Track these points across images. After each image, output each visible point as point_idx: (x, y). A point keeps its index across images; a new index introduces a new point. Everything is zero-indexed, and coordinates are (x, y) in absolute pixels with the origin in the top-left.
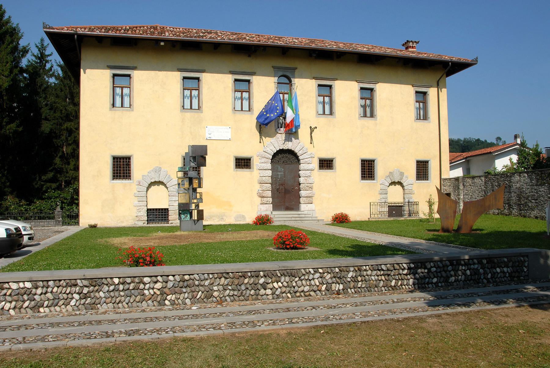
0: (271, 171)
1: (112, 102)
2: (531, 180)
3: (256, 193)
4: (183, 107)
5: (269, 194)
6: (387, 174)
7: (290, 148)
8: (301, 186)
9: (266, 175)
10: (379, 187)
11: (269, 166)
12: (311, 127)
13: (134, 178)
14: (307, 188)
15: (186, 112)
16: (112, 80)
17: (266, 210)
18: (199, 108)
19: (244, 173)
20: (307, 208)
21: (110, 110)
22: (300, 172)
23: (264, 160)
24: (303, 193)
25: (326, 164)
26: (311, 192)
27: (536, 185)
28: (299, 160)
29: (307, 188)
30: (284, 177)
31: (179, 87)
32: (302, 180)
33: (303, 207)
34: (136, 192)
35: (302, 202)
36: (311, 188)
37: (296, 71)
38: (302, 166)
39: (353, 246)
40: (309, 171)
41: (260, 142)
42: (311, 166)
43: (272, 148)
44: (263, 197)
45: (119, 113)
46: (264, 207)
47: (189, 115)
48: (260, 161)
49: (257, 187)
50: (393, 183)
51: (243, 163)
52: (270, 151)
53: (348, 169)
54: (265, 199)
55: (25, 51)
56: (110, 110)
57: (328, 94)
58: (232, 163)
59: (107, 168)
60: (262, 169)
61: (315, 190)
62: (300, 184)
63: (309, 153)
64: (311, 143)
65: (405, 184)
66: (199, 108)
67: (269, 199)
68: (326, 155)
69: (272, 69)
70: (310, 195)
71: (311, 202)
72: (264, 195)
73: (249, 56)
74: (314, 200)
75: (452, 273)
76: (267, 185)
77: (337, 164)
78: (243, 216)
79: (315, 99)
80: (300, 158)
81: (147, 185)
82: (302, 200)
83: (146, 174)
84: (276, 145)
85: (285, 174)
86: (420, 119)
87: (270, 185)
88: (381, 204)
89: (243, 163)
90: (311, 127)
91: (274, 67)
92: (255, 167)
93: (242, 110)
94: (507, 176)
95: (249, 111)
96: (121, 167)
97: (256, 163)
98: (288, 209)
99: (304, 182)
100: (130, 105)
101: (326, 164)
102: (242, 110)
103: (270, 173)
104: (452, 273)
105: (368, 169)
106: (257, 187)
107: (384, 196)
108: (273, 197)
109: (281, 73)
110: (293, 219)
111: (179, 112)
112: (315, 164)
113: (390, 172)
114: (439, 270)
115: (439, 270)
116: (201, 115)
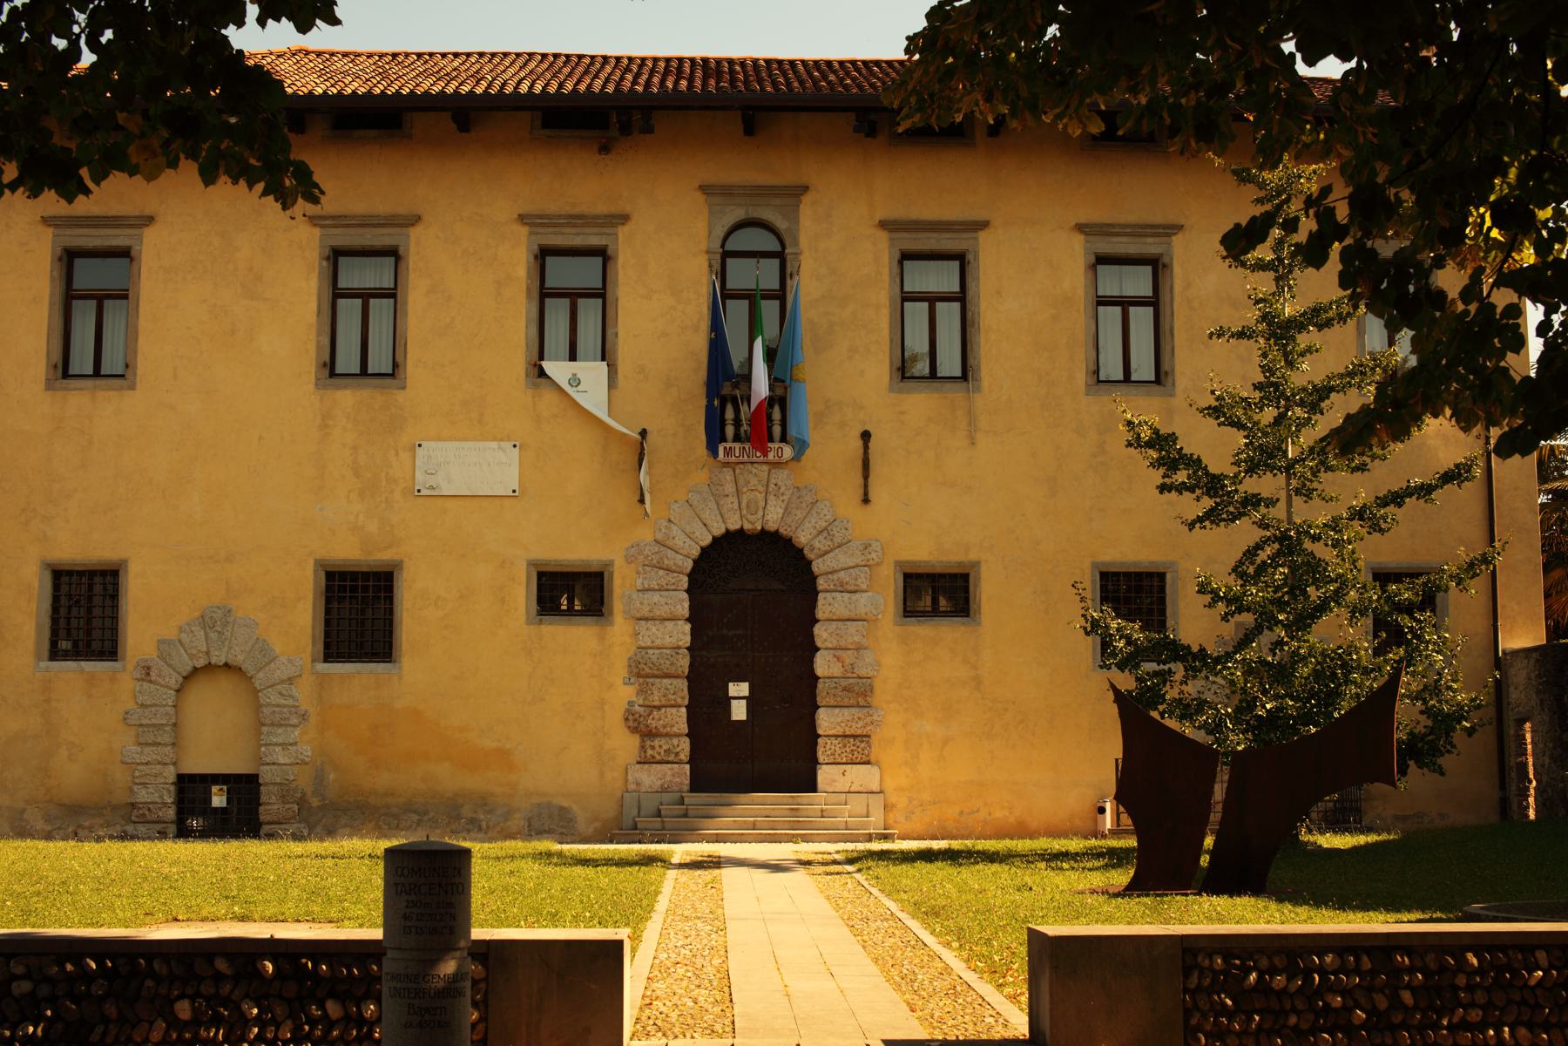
1: (57, 356)
4: (1097, 372)
13: (129, 653)
15: (338, 387)
16: (896, 269)
19: (574, 636)
21: (49, 386)
23: (661, 577)
24: (827, 720)
25: (940, 593)
31: (315, 291)
34: (130, 705)
37: (807, 199)
40: (857, 627)
42: (862, 603)
45: (79, 399)
46: (650, 778)
47: (347, 398)
51: (568, 592)
57: (1145, 290)
58: (522, 595)
60: (653, 619)
66: (966, 374)
68: (926, 552)
73: (605, 149)
75: (111, 1010)
81: (174, 680)
83: (171, 633)
89: (568, 592)
91: (705, 189)
93: (1127, 378)
99: (836, 670)
100: (395, 365)
101: (940, 593)
102: (1127, 378)
104: (111, 1010)
106: (624, 694)
109: (737, 214)
111: (311, 387)
112: (885, 597)
114: (44, 990)
115: (44, 990)
116: (401, 397)
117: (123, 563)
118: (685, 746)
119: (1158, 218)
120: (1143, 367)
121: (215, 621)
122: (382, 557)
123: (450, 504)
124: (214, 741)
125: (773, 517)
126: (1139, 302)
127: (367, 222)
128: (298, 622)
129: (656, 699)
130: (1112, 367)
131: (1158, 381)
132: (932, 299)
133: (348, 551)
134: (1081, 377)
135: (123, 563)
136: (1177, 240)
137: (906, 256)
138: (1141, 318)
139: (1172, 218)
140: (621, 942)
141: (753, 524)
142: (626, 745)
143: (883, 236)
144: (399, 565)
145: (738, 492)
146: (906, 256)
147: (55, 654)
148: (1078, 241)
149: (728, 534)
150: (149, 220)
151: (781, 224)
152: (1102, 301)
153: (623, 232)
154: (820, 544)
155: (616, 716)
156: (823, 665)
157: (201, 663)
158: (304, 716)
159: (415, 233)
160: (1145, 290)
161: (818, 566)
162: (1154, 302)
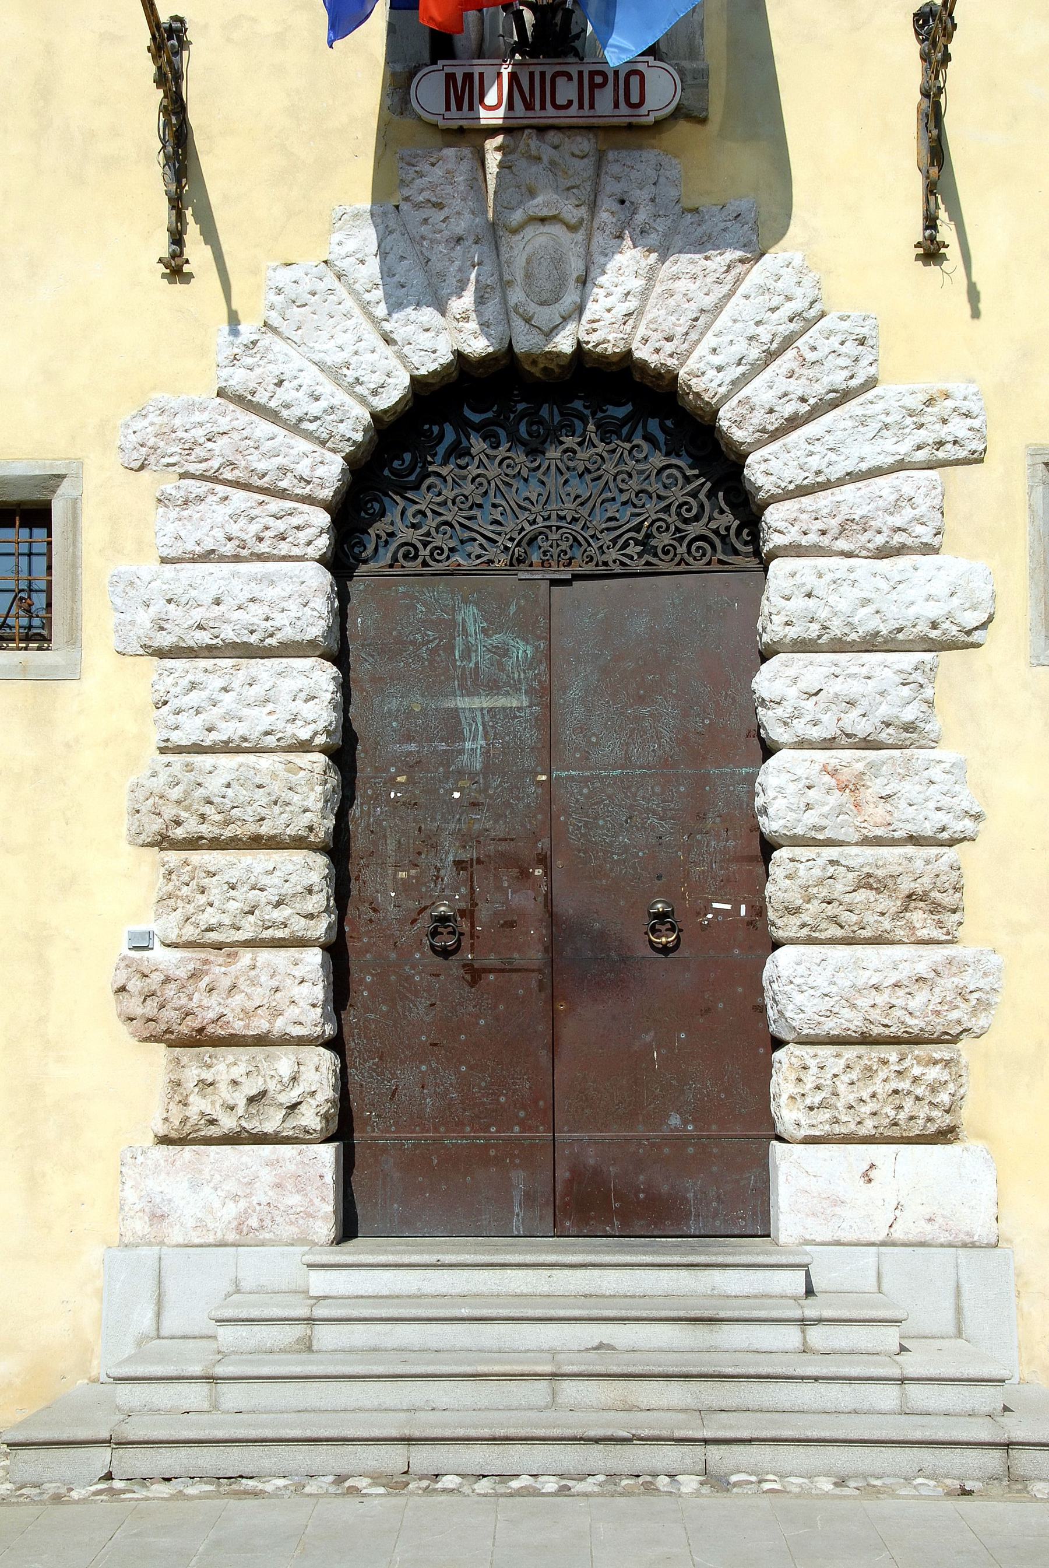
3: (108, 978)
5: (296, 988)
8: (786, 878)
9: (254, 723)
11: (299, 595)
14: (874, 910)
17: (244, 1237)
20: (867, 1212)
22: (767, 681)
23: (221, 516)
24: (801, 982)
26: (925, 959)
28: (749, 509)
29: (874, 910)
30: (548, 750)
32: (785, 792)
33: (815, 1188)
35: (788, 1114)
36: (936, 905)
38: (788, 593)
41: (176, 270)
44: (199, 1039)
48: (170, 530)
52: (307, 390)
54: (228, 1065)
55: (498, 149)
56: (1034, 452)
62: (768, 847)
63: (894, 394)
64: (931, 253)
67: (284, 1061)
70: (917, 1011)
71: (922, 1115)
72: (209, 1008)
74: (988, 1081)
76: (259, 861)
80: (763, 470)
82: (793, 1085)
85: (547, 719)
98: (599, 1205)
99: (825, 810)
106: (122, 896)
110: (588, 1403)
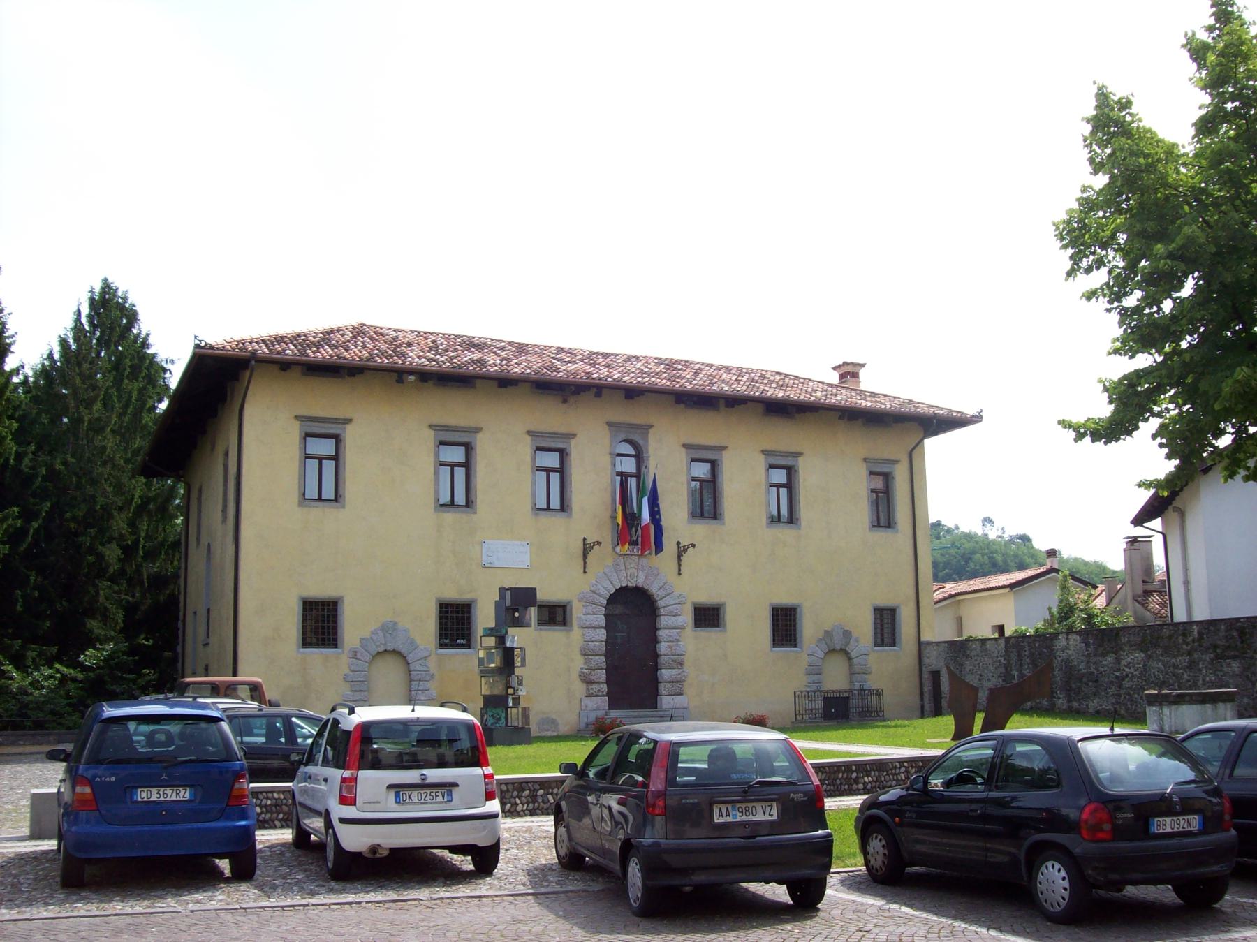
0: (604, 631)
2: (1087, 645)
5: (602, 675)
6: (821, 635)
7: (640, 585)
10: (804, 660)
12: (678, 543)
17: (598, 709)
18: (337, 499)
23: (593, 608)
24: (665, 673)
25: (708, 616)
27: (1095, 655)
34: (347, 671)
36: (681, 664)
39: (473, 386)
40: (677, 634)
42: (680, 620)
43: (607, 584)
46: (592, 703)
47: (450, 517)
49: (579, 662)
50: (831, 651)
53: (748, 628)
54: (594, 686)
57: (784, 481)
59: (291, 624)
61: (689, 668)
65: (853, 654)
66: (337, 499)
68: (704, 598)
69: (607, 427)
73: (565, 401)
74: (686, 687)
77: (730, 615)
78: (554, 722)
79: (685, 486)
83: (367, 634)
84: (614, 578)
86: (702, 516)
87: (603, 659)
88: (808, 695)
90: (678, 543)
91: (609, 424)
92: (575, 623)
93: (320, 498)
94: (1046, 639)
95: (336, 500)
96: (321, 623)
97: (577, 612)
99: (668, 651)
102: (320, 498)
103: (602, 634)
105: (784, 624)
107: (815, 678)
108: (608, 682)
109: (623, 437)
112: (687, 617)
113: (826, 632)
117: (341, 598)
118: (605, 688)
119: (793, 449)
120: (328, 492)
121: (389, 628)
122: (467, 597)
123: (499, 571)
124: (836, 680)
125: (640, 580)
126: (554, 470)
127: (457, 429)
128: (426, 629)
129: (593, 665)
130: (312, 492)
131: (336, 500)
132: (321, 459)
133: (452, 594)
134: (295, 497)
135: (341, 598)
136: (800, 459)
137: (308, 435)
138: (329, 466)
139: (799, 449)
140: (35, 797)
141: (632, 584)
142: (580, 688)
143: (683, 450)
144: (474, 601)
145: (626, 569)
146: (308, 435)
147: (305, 644)
148: (762, 457)
149: (622, 588)
150: (349, 421)
151: (641, 442)
152: (309, 457)
153: (573, 442)
154: (661, 593)
155: (575, 675)
156: (663, 648)
157: (381, 649)
158: (432, 676)
159: (479, 436)
160: (784, 481)
161: (660, 603)
162: (336, 458)
